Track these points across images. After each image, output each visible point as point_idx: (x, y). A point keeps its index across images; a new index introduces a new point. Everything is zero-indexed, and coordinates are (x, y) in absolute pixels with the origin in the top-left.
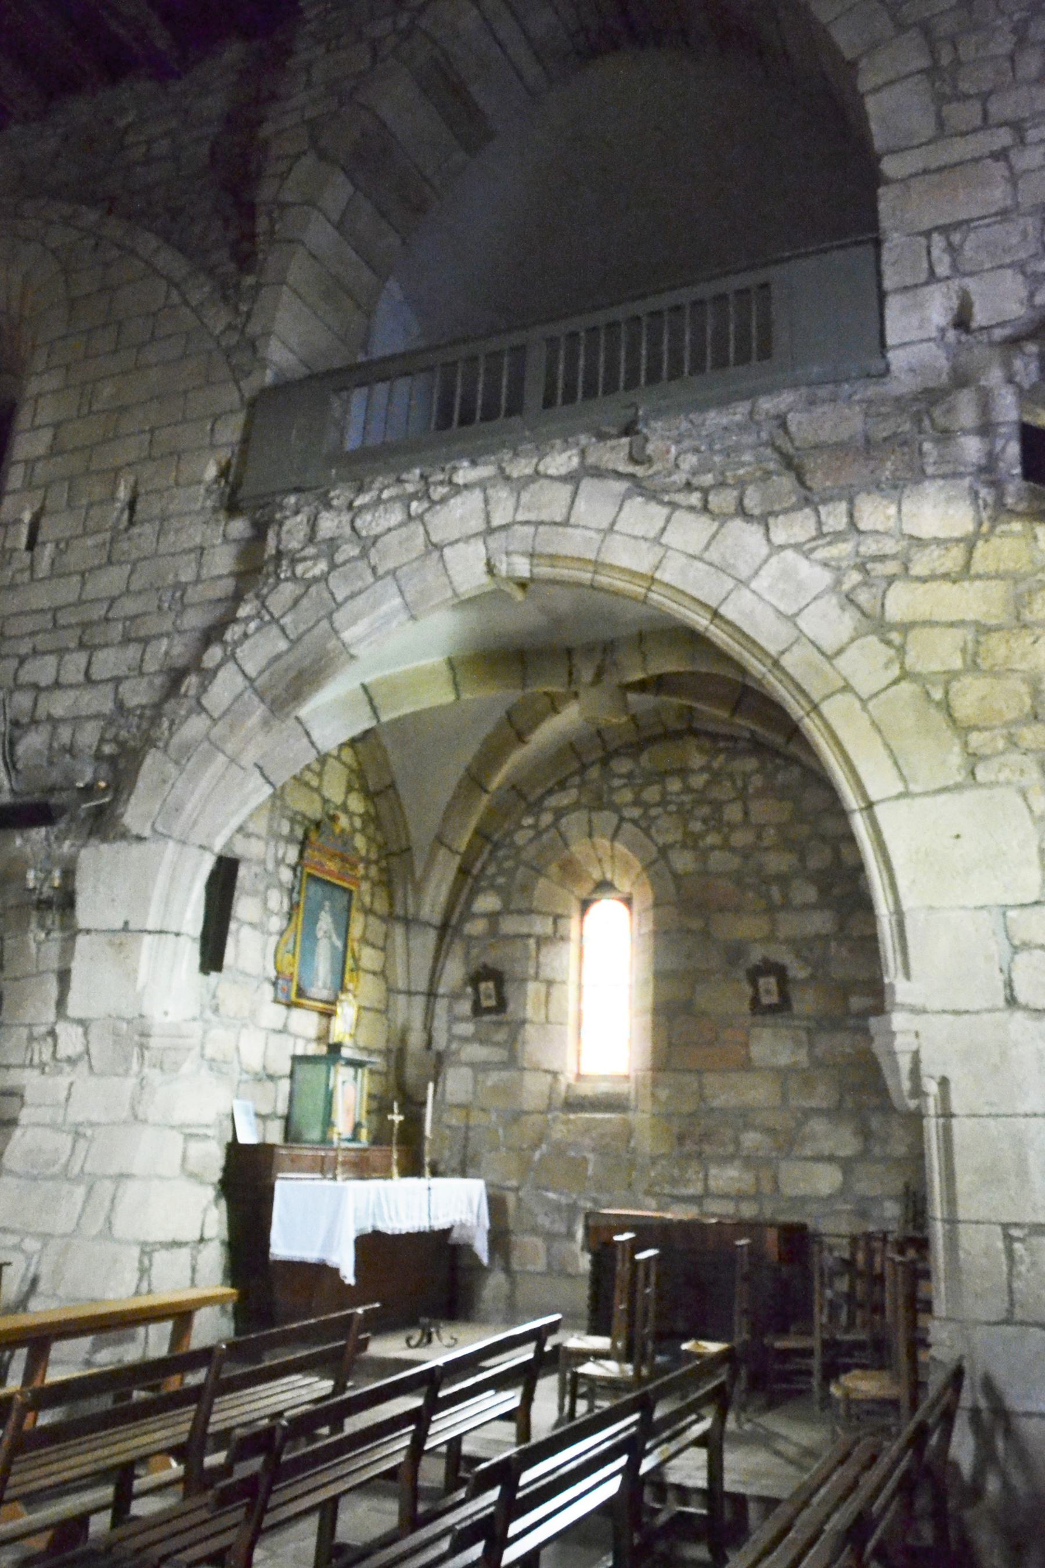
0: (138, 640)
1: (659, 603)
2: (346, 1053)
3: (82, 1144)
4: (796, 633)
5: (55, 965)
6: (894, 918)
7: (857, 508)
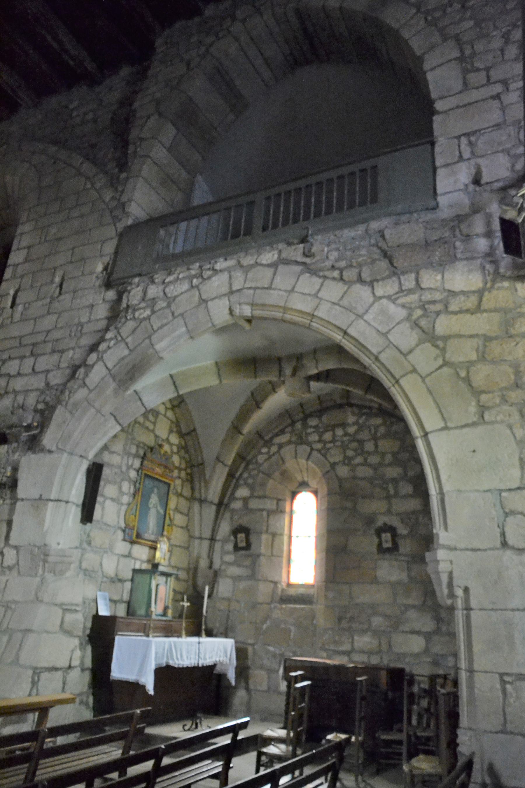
0: (59, 351)
1: (316, 328)
2: (161, 568)
3: (9, 613)
4: (388, 342)
5: (6, 517)
6: (439, 496)
7: (420, 276)
